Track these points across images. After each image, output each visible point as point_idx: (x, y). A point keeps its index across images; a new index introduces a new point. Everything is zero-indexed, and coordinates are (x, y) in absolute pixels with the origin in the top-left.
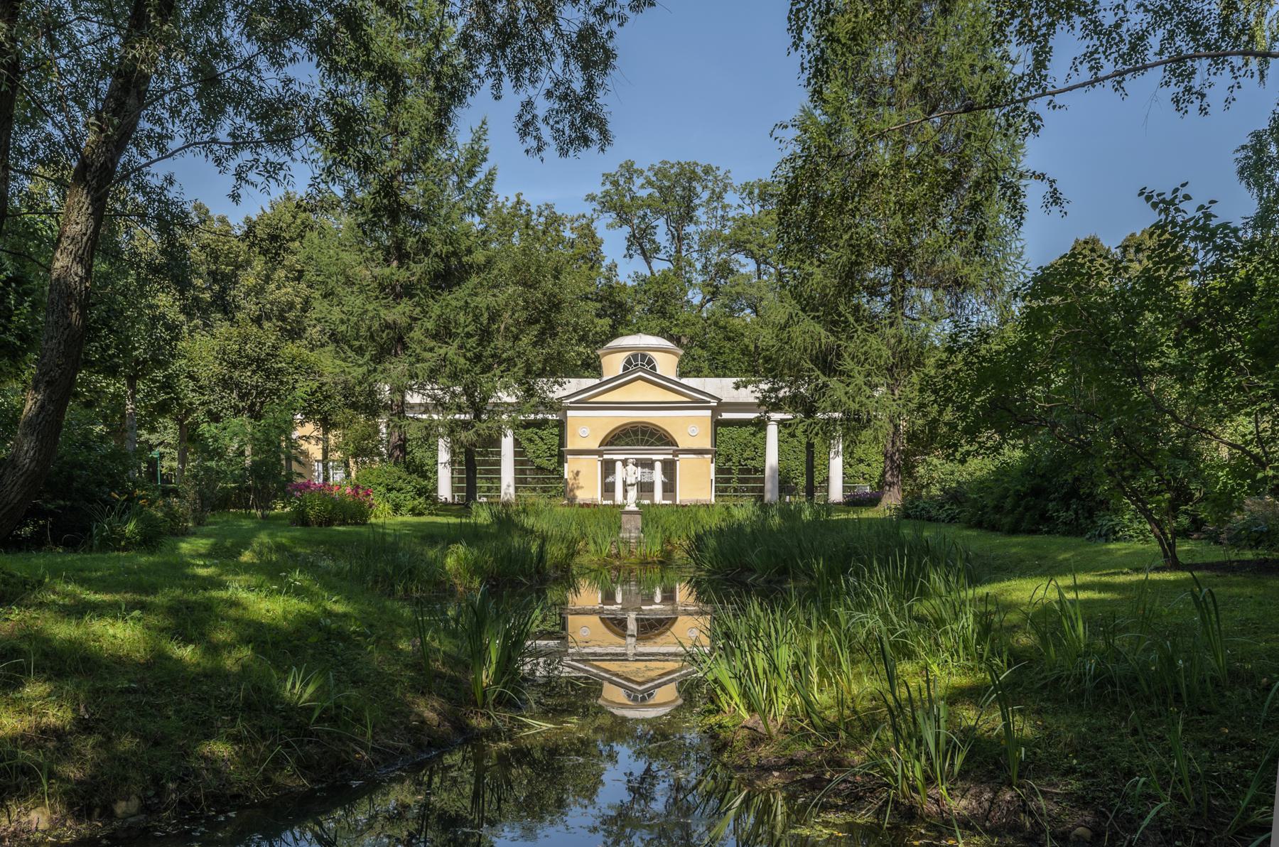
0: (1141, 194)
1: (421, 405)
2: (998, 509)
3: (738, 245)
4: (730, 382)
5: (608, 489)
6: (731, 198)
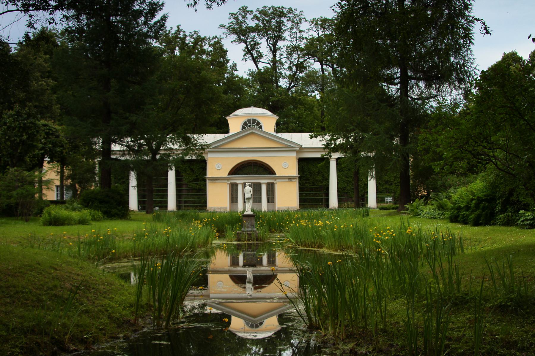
0: (529, 37)
1: (120, 151)
2: (467, 208)
3: (311, 55)
4: (307, 135)
5: (234, 199)
6: (304, 26)
